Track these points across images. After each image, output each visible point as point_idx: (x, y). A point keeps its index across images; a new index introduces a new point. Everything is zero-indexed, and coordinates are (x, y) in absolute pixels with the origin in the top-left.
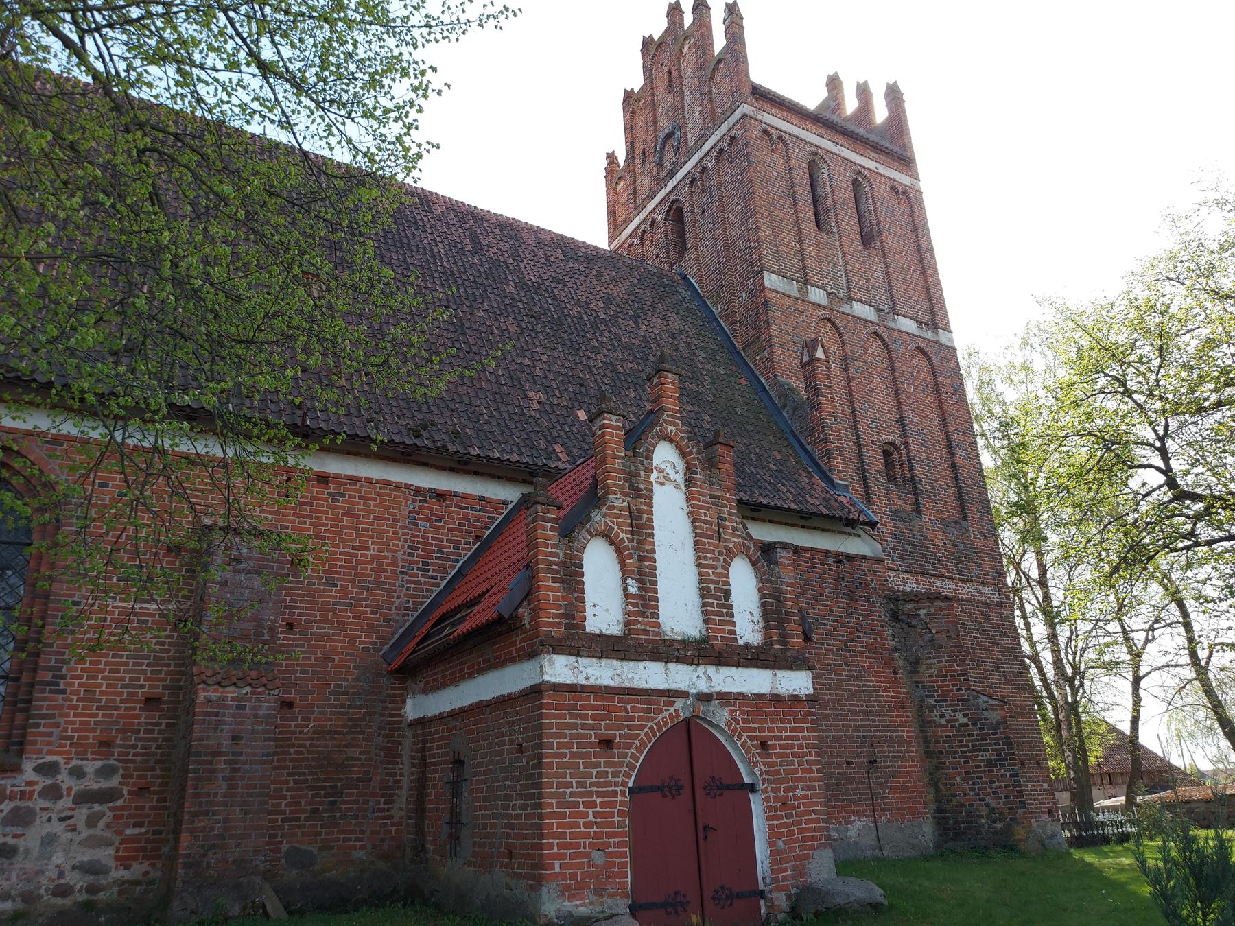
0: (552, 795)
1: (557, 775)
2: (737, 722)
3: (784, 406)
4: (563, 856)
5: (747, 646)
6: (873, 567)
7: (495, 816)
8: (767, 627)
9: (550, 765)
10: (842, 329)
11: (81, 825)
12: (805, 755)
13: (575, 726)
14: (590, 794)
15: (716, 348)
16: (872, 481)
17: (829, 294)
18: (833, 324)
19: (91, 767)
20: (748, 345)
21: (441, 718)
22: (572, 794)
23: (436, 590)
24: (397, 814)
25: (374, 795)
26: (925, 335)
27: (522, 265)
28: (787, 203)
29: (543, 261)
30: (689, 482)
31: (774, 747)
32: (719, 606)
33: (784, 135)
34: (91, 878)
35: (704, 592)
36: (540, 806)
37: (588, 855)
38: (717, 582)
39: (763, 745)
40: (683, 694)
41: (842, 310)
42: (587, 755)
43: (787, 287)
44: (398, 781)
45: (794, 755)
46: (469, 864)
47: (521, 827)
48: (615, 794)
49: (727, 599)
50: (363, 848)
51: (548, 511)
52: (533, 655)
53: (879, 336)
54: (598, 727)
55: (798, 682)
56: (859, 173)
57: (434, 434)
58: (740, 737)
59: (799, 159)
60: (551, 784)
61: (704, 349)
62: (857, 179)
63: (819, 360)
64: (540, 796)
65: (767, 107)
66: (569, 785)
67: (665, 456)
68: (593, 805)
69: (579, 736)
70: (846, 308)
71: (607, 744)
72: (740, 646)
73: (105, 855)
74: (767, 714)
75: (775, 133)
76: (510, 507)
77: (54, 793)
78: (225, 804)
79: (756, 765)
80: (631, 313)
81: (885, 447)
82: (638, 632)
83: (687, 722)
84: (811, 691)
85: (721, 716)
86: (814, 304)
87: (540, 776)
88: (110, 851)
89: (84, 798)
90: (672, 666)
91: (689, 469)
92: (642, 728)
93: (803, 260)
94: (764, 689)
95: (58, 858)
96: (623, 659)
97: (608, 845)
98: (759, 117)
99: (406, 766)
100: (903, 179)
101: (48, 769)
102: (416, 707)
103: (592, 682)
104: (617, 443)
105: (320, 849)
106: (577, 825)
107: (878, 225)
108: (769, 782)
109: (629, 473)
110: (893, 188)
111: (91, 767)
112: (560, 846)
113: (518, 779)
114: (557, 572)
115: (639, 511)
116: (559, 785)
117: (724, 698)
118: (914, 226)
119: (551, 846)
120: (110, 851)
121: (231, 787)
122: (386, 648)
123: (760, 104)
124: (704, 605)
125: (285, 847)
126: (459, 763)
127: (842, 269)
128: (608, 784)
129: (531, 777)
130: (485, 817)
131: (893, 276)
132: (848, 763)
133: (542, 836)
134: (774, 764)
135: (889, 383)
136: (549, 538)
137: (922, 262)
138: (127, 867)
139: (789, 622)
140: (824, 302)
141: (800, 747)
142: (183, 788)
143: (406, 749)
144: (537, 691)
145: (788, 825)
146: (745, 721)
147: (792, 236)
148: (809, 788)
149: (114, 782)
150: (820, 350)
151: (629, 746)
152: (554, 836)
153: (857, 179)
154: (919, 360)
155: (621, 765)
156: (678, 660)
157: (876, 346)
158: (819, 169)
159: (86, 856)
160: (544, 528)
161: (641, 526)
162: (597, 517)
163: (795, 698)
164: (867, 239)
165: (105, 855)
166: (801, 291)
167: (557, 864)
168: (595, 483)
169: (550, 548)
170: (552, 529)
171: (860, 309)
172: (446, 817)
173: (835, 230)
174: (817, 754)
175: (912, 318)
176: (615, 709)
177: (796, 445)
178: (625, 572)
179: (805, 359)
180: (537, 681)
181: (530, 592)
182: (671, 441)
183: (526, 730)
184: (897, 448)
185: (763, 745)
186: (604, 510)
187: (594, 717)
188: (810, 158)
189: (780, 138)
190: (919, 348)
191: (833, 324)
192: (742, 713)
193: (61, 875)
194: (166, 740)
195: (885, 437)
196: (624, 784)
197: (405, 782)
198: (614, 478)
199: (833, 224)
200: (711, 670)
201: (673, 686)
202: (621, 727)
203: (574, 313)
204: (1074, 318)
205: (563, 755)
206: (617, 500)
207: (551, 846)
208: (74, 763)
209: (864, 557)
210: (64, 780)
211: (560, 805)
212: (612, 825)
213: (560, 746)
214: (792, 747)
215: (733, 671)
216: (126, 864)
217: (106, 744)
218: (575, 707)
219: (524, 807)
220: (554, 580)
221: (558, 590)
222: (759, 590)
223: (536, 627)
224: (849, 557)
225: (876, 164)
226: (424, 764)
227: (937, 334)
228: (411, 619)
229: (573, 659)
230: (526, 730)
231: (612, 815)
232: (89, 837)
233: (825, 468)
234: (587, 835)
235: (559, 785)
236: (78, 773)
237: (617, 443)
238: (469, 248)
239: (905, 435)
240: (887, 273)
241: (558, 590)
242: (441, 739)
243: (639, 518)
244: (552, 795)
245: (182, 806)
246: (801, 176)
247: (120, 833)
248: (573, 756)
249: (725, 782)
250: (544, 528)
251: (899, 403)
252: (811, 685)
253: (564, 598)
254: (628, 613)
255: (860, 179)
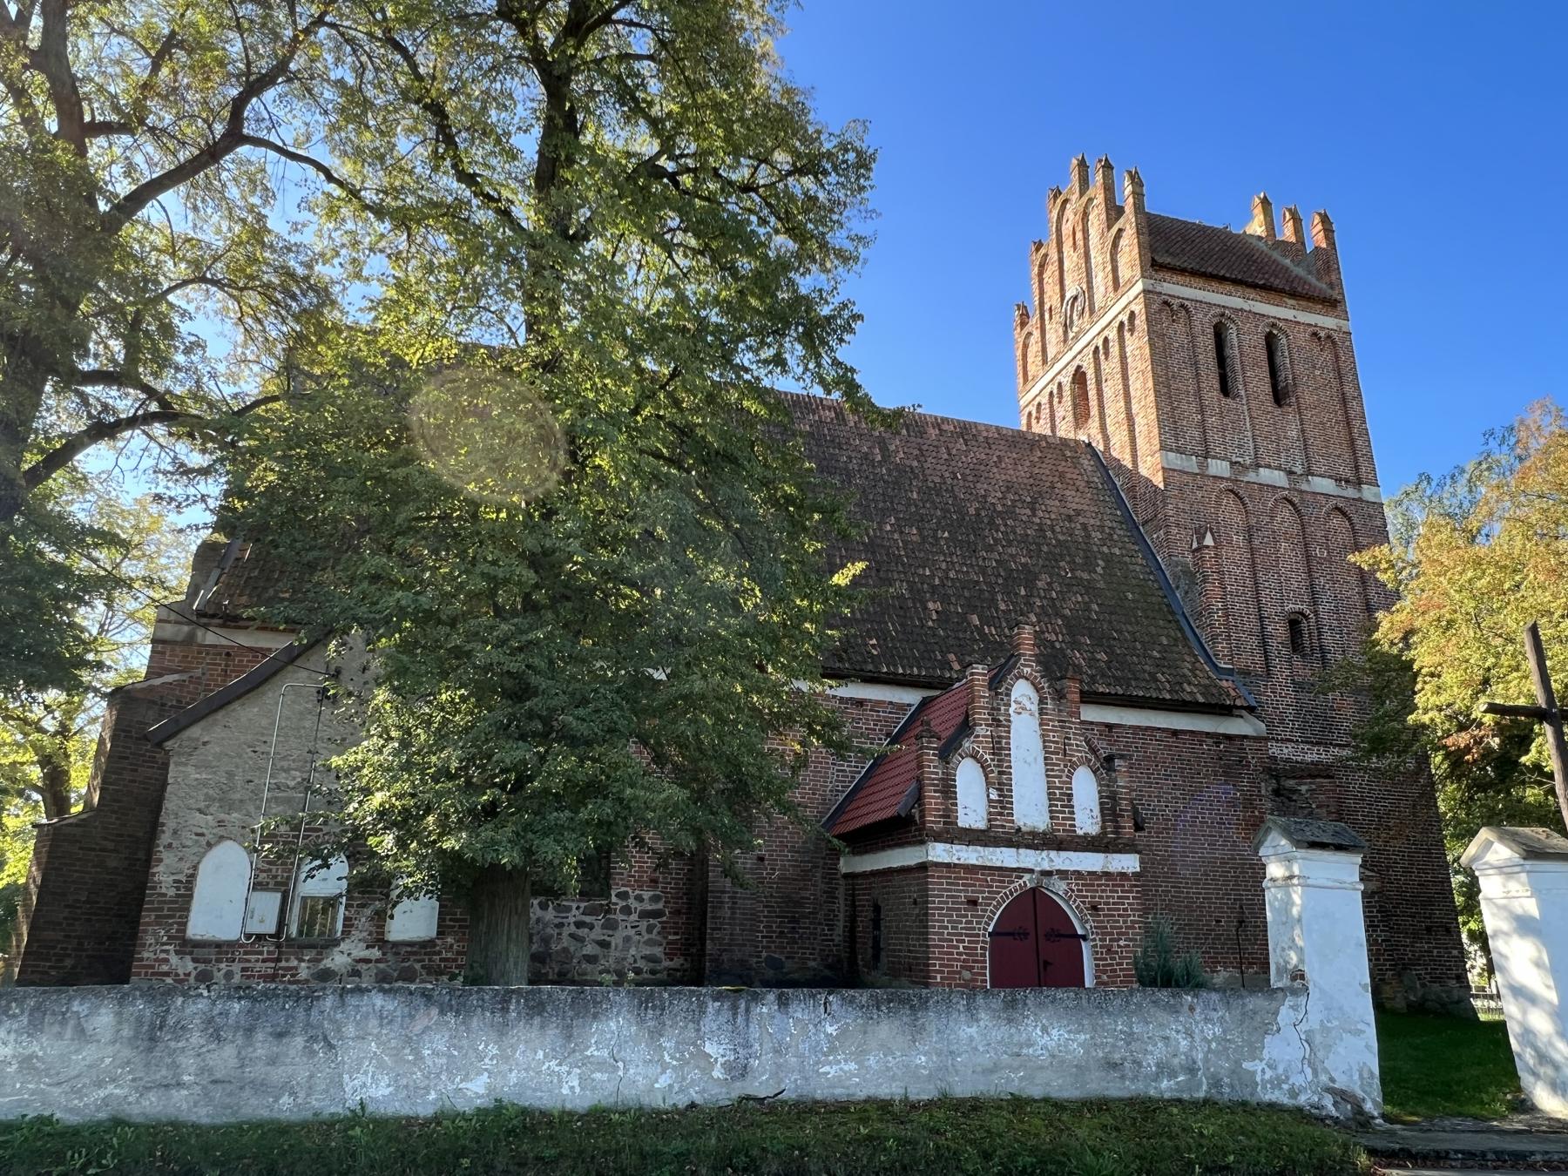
0: (935, 934)
1: (938, 921)
2: (1073, 891)
3: (1178, 587)
4: (943, 972)
5: (1086, 836)
6: (1256, 745)
7: (901, 944)
8: (1104, 821)
9: (934, 915)
10: (1247, 500)
11: (644, 932)
12: (1129, 916)
13: (950, 890)
14: (961, 935)
15: (1115, 525)
16: (1273, 654)
17: (1233, 464)
18: (1236, 495)
19: (646, 895)
20: (1146, 522)
21: (864, 875)
22: (949, 934)
23: (858, 777)
24: (837, 939)
25: (820, 924)
26: (1344, 493)
27: (926, 466)
28: (1188, 373)
29: (945, 456)
30: (1042, 712)
31: (1103, 909)
32: (1062, 806)
33: (1186, 303)
34: (651, 965)
35: (1051, 796)
36: (927, 940)
37: (959, 973)
38: (1062, 788)
39: (1094, 908)
40: (1031, 871)
41: (1246, 479)
42: (959, 909)
43: (1185, 464)
44: (835, 916)
45: (1119, 915)
46: (886, 974)
47: (917, 952)
48: (978, 935)
49: (1069, 801)
50: (815, 960)
51: (930, 742)
52: (922, 842)
53: (1291, 502)
54: (967, 891)
55: (1128, 863)
56: (1274, 325)
57: (853, 656)
58: (1075, 901)
59: (1203, 324)
60: (934, 927)
61: (1101, 528)
62: (1271, 332)
63: (1207, 547)
64: (927, 933)
65: (1167, 276)
66: (947, 928)
67: (1022, 692)
68: (963, 941)
69: (953, 897)
70: (1251, 476)
71: (973, 903)
72: (1079, 837)
73: (658, 951)
74: (1098, 885)
75: (1175, 302)
76: (913, 709)
77: (627, 910)
78: (729, 924)
79: (1087, 922)
80: (1029, 499)
81: (1292, 617)
82: (997, 826)
83: (1033, 890)
84: (1138, 870)
85: (1060, 886)
86: (1214, 477)
87: (927, 921)
88: (661, 949)
89: (645, 915)
90: (1022, 851)
91: (1042, 701)
92: (999, 893)
93: (1204, 432)
94: (1098, 868)
95: (633, 951)
96: (986, 845)
97: (973, 967)
98: (1159, 289)
99: (841, 905)
100: (1327, 322)
101: (623, 896)
102: (848, 864)
103: (962, 862)
104: (982, 686)
105: (787, 958)
106: (952, 954)
107: (1294, 379)
108: (1097, 934)
109: (993, 709)
110: (1315, 334)
111: (646, 895)
112: (941, 965)
113: (914, 921)
114: (937, 785)
115: (999, 737)
116: (940, 927)
117: (1063, 874)
118: (1339, 373)
119: (935, 965)
120: (661, 949)
121: (733, 913)
122: (824, 820)
123: (1161, 275)
124: (1050, 806)
125: (764, 954)
126: (877, 909)
127: (1250, 434)
128: (974, 929)
129: (921, 921)
130: (894, 944)
131: (1309, 434)
132: (1218, 921)
133: (929, 958)
134: (1103, 922)
135: (1299, 550)
136: (932, 761)
137: (1346, 412)
138: (672, 960)
139: (1123, 816)
140: (1227, 474)
141: (1125, 910)
142: (705, 913)
143: (841, 893)
144: (923, 867)
145: (1112, 965)
146: (1078, 890)
147: (1194, 407)
148: (1131, 940)
149: (660, 906)
150: (1209, 535)
151: (989, 905)
152: (937, 959)
153: (1271, 332)
154: (1337, 521)
155: (983, 917)
156: (1028, 847)
157: (1285, 513)
158: (1227, 329)
159: (647, 951)
160: (928, 754)
161: (1002, 749)
162: (967, 744)
163: (1123, 875)
164: (1280, 396)
165: (658, 951)
166: (1200, 465)
167: (939, 976)
168: (967, 716)
169: (933, 769)
170: (934, 755)
171: (1267, 476)
172: (870, 943)
173: (1243, 393)
174: (1139, 916)
175: (1330, 477)
176: (978, 880)
177: (1186, 628)
178: (989, 784)
179: (1195, 545)
180: (924, 860)
181: (919, 798)
182: (1027, 679)
183: (919, 891)
184: (1306, 617)
185: (1094, 908)
186: (972, 739)
187: (963, 885)
188: (1215, 321)
189: (1182, 306)
190: (1337, 508)
191: (1236, 495)
192: (1077, 884)
193: (635, 961)
194: (688, 879)
195: (1290, 607)
196: (985, 929)
197: (841, 916)
198: (980, 713)
199: (1241, 387)
200: (1053, 854)
201: (1022, 865)
202: (984, 892)
203: (972, 511)
204: (734, 1009)
205: (943, 909)
206: (981, 730)
207: (935, 965)
208: (637, 892)
209: (1245, 737)
210: (632, 903)
211: (940, 940)
212: (977, 955)
213: (940, 902)
214: (1119, 910)
215: (1071, 854)
216: (671, 958)
217: (654, 881)
218: (950, 878)
219: (918, 940)
220: (935, 791)
221: (938, 798)
222: (1099, 792)
223: (924, 823)
224: (1229, 737)
225: (1294, 312)
226: (853, 906)
227: (1360, 491)
228: (841, 799)
229: (948, 846)
230: (919, 891)
231: (976, 949)
232: (649, 939)
233: (1211, 653)
234: (959, 960)
235: (940, 927)
236: (639, 899)
237: (982, 686)
238: (879, 458)
239: (1314, 602)
240: (1303, 431)
241: (938, 798)
242: (866, 889)
243: (1000, 743)
244: (935, 934)
245: (705, 924)
246: (1207, 342)
247: (666, 938)
248: (949, 909)
249: (1062, 932)
250: (928, 754)
251: (1310, 571)
252: (1137, 865)
253: (942, 804)
254: (990, 813)
255: (1275, 332)
